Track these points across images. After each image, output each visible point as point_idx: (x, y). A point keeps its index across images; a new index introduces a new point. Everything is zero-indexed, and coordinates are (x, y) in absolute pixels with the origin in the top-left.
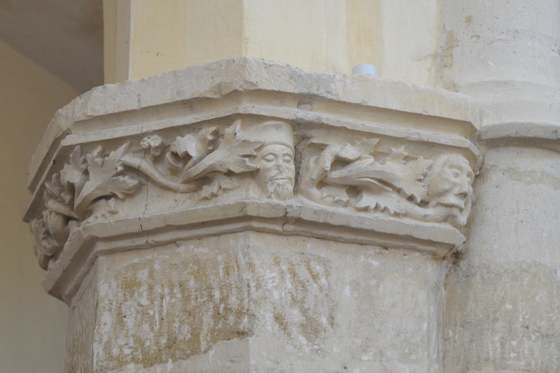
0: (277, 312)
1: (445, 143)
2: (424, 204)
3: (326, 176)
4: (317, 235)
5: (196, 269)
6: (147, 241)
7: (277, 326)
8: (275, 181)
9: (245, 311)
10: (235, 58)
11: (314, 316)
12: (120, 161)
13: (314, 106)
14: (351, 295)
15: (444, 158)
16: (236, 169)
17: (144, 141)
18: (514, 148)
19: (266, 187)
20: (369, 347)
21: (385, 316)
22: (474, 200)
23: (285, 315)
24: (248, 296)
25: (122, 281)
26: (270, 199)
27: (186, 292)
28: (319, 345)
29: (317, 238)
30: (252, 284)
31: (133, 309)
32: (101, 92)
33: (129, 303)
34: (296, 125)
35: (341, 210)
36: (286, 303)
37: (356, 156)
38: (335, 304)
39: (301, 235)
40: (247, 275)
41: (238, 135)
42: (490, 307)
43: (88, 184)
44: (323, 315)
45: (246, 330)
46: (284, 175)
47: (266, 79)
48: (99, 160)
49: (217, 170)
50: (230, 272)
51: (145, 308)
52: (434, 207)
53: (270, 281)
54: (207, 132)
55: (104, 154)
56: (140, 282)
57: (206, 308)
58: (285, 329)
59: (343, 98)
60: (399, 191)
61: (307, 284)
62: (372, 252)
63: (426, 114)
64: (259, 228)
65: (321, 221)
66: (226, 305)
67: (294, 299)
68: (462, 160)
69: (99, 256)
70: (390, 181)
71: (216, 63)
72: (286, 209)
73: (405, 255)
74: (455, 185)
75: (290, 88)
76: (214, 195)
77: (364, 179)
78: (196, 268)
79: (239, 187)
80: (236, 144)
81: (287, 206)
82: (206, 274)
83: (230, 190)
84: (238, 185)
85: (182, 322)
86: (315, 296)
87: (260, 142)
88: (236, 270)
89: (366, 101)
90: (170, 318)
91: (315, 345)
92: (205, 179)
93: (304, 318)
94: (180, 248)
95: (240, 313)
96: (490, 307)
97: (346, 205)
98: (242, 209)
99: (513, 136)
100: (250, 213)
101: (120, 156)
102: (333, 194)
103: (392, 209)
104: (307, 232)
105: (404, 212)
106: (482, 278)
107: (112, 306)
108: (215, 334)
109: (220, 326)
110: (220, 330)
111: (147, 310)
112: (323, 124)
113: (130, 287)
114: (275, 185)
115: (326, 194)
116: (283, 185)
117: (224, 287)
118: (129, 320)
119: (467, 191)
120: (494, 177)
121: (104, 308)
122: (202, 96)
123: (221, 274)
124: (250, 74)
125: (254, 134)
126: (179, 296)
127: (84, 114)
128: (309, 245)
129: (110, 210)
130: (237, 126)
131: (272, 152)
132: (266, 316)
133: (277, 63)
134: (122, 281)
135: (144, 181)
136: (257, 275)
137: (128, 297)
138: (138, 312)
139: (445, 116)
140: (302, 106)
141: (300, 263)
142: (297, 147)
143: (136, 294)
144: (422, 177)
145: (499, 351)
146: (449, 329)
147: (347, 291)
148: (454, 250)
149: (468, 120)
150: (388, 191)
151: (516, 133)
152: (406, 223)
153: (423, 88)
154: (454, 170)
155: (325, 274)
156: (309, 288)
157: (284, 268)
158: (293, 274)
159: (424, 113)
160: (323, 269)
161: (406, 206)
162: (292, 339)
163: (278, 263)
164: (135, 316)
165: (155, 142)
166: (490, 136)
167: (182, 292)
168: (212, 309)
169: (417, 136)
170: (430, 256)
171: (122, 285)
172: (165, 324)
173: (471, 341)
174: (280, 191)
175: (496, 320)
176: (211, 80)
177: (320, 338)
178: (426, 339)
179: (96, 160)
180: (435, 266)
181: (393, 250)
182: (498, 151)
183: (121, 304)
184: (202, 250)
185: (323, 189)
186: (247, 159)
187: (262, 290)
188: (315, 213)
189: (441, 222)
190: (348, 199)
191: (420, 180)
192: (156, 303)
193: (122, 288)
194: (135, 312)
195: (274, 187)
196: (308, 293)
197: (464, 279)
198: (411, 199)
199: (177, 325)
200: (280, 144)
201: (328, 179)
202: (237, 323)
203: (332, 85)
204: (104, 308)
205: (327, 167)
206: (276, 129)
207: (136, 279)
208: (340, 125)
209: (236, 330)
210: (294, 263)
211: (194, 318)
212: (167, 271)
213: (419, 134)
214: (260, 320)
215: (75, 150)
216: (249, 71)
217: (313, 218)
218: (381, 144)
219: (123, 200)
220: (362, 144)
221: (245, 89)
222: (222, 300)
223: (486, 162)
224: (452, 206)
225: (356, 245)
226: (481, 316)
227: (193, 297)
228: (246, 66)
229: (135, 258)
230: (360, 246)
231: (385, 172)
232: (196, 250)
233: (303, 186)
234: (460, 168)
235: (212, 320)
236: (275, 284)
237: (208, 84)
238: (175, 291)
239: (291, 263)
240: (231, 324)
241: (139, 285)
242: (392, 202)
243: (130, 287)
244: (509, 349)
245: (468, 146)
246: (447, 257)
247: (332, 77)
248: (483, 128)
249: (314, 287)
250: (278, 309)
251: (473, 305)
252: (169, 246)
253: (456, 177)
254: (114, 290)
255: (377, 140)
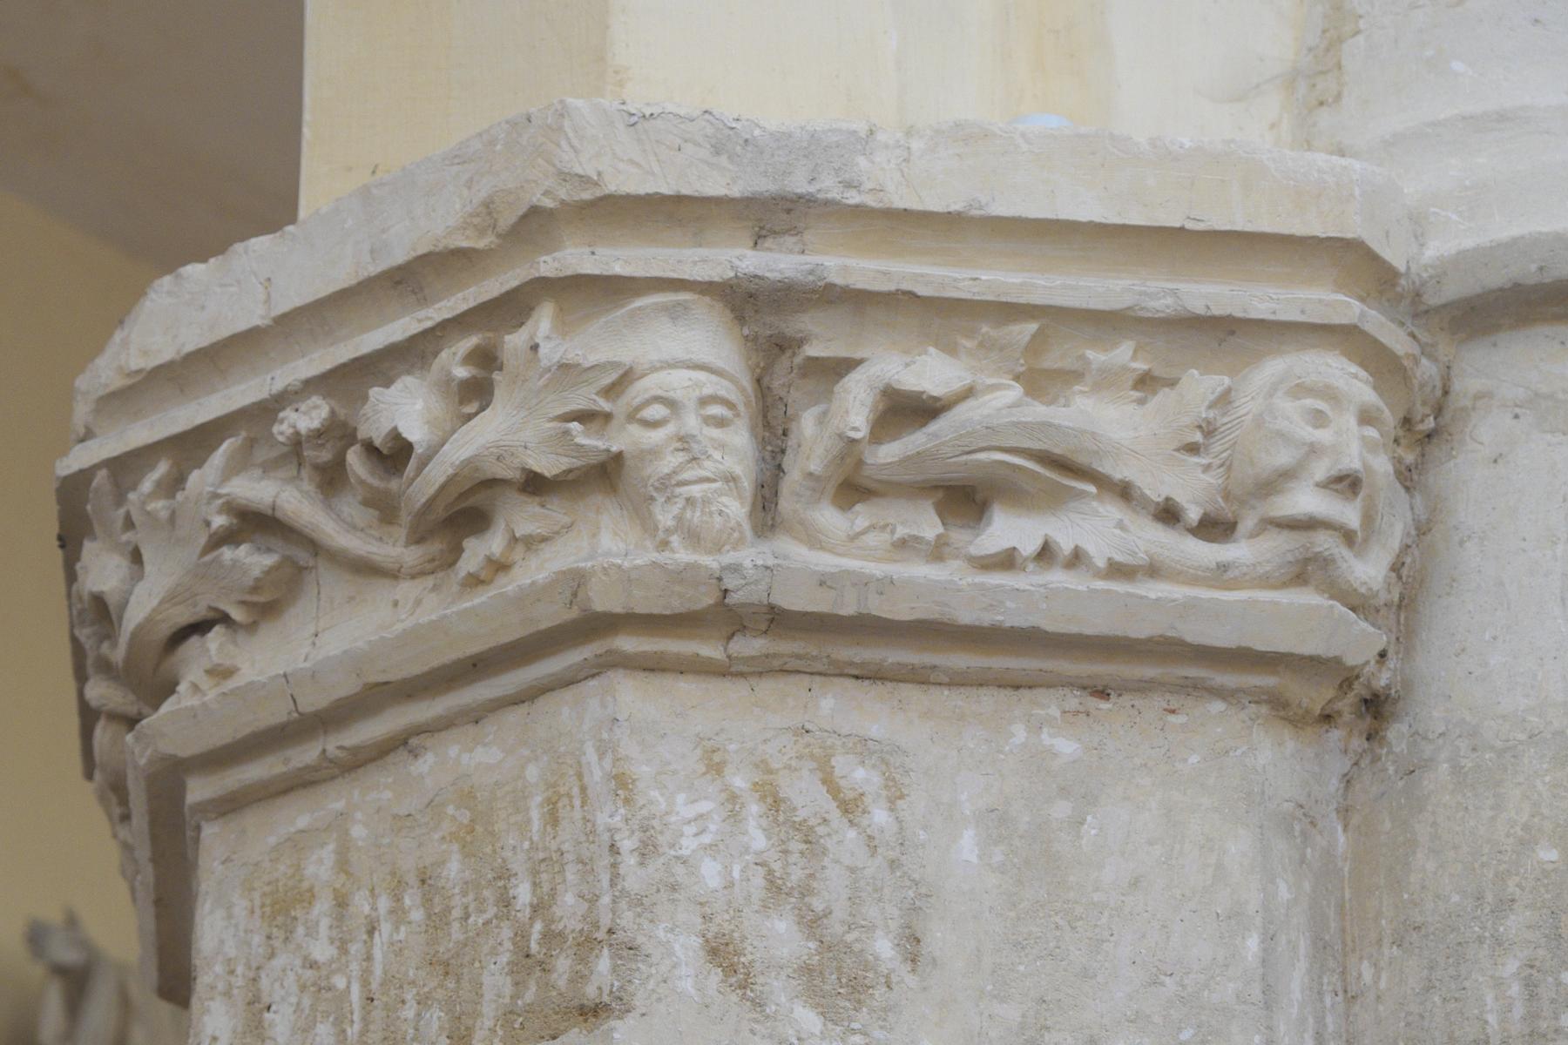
0: (714, 929)
1: (1272, 317)
2: (1215, 528)
3: (860, 463)
4: (852, 664)
5: (466, 822)
6: (324, 751)
7: (716, 976)
8: (678, 490)
9: (601, 935)
10: (533, 110)
11: (849, 938)
12: (216, 496)
13: (807, 236)
14: (979, 857)
15: (1275, 367)
16: (548, 464)
17: (282, 422)
18: (1547, 329)
19: (650, 514)
20: (1048, 1028)
21: (1104, 920)
22: (1423, 518)
23: (744, 938)
24: (613, 884)
25: (264, 894)
26: (667, 554)
27: (437, 900)
28: (865, 1034)
29: (857, 677)
30: (627, 844)
31: (291, 977)
32: (169, 293)
33: (279, 962)
34: (742, 300)
35: (921, 571)
36: (748, 898)
37: (957, 386)
38: (923, 890)
39: (799, 672)
40: (608, 816)
41: (542, 351)
42: (1483, 865)
43: (141, 589)
44: (879, 933)
45: (606, 999)
46: (708, 468)
47: (632, 162)
48: (159, 506)
49: (489, 476)
50: (562, 813)
51: (324, 972)
52: (1253, 535)
53: (690, 830)
54: (454, 361)
55: (175, 483)
56: (311, 890)
57: (491, 942)
58: (743, 986)
59: (901, 199)
60: (1125, 492)
61: (821, 830)
62: (1054, 711)
63: (1200, 227)
64: (644, 655)
65: (848, 610)
66: (549, 922)
67: (775, 887)
68: (1337, 370)
69: (203, 823)
70: (1082, 459)
71: (480, 135)
72: (720, 579)
73: (1173, 712)
74: (1313, 450)
75: (714, 185)
76: (500, 566)
77: (982, 456)
78: (465, 817)
79: (570, 527)
80: (541, 383)
81: (723, 569)
82: (492, 834)
83: (544, 539)
84: (567, 520)
85: (423, 1001)
86: (852, 870)
87: (615, 365)
88: (577, 802)
89: (984, 201)
90: (393, 992)
91: (854, 1032)
92: (464, 511)
93: (812, 945)
94: (421, 761)
95: (587, 945)
96: (1483, 865)
97: (938, 552)
98: (575, 595)
99: (1532, 282)
100: (600, 604)
101: (221, 482)
102: (892, 521)
103: (1099, 553)
104: (814, 658)
105: (1142, 558)
106: (1456, 769)
107: (233, 979)
108: (517, 1026)
109: (530, 995)
110: (529, 1010)
111: (328, 978)
112: (830, 286)
113: (283, 909)
114: (681, 503)
115: (867, 524)
116: (706, 501)
117: (543, 866)
118: (277, 1018)
119: (1356, 465)
120: (1485, 432)
121: (213, 988)
122: (441, 247)
123: (536, 825)
124: (576, 151)
125: (601, 343)
126: (417, 915)
127: (120, 369)
128: (827, 704)
129: (208, 666)
130: (543, 322)
131: (660, 393)
132: (677, 947)
133: (670, 108)
134: (264, 894)
135: (303, 557)
136: (644, 812)
137: (277, 943)
138: (303, 988)
139: (1265, 225)
140: (769, 243)
141: (793, 763)
142: (766, 381)
143: (301, 930)
144: (1198, 437)
145: (1519, 1011)
146: (1361, 958)
147: (968, 845)
148: (1359, 689)
149: (1349, 235)
150: (1081, 494)
151: (1541, 269)
152: (1153, 596)
153: (1188, 144)
154: (1309, 402)
155: (884, 793)
156: (829, 843)
157: (739, 782)
158: (770, 800)
159: (1190, 225)
160: (876, 779)
161: (1152, 539)
162: (768, 1017)
163: (715, 767)
164: (294, 1000)
165: (308, 417)
166: (1453, 290)
167: (427, 901)
168: (508, 945)
169: (1169, 301)
170: (1264, 709)
171: (263, 905)
172: (378, 1014)
173: (1429, 988)
174: (696, 520)
175: (1505, 905)
176: (465, 192)
177: (872, 1011)
178: (1256, 990)
179: (150, 507)
180: (1290, 745)
181: (1126, 700)
182: (1495, 345)
183: (258, 968)
184: (474, 757)
185: (859, 507)
186: (575, 426)
187: (662, 860)
188: (822, 584)
189: (1284, 585)
190: (941, 530)
191: (1193, 449)
192: (354, 948)
193: (262, 917)
194: (295, 988)
195: (676, 509)
196: (826, 861)
197: (1401, 784)
198: (1168, 514)
199: (409, 1012)
200: (688, 367)
201: (867, 472)
202: (578, 978)
203: (862, 162)
204: (213, 988)
205: (855, 429)
206: (674, 319)
207: (301, 881)
208: (892, 287)
209: (576, 1002)
210: (775, 766)
211: (458, 982)
212: (386, 841)
213: (1174, 293)
214: (653, 960)
215: (94, 484)
216: (576, 142)
217: (817, 602)
218: (1049, 340)
219: (251, 628)
220: (981, 345)
221: (563, 202)
222: (537, 909)
223: (1457, 386)
224: (1309, 524)
225: (995, 691)
226: (1456, 898)
227: (457, 913)
228: (560, 129)
229: (298, 816)
230: (1009, 692)
231: (1058, 427)
232: (465, 758)
233: (786, 504)
234: (1330, 394)
235: (509, 979)
236: (706, 839)
237: (458, 206)
238: (407, 901)
239: (764, 766)
240: (562, 984)
241: (308, 897)
242: (1096, 528)
243: (283, 909)
244: (1553, 1001)
245: (1355, 321)
246: (1339, 713)
247: (863, 134)
248: (1426, 267)
249: (845, 841)
250: (718, 920)
251: (1431, 866)
252: (390, 758)
253: (1316, 427)
254: (241, 928)
255: (1033, 327)
